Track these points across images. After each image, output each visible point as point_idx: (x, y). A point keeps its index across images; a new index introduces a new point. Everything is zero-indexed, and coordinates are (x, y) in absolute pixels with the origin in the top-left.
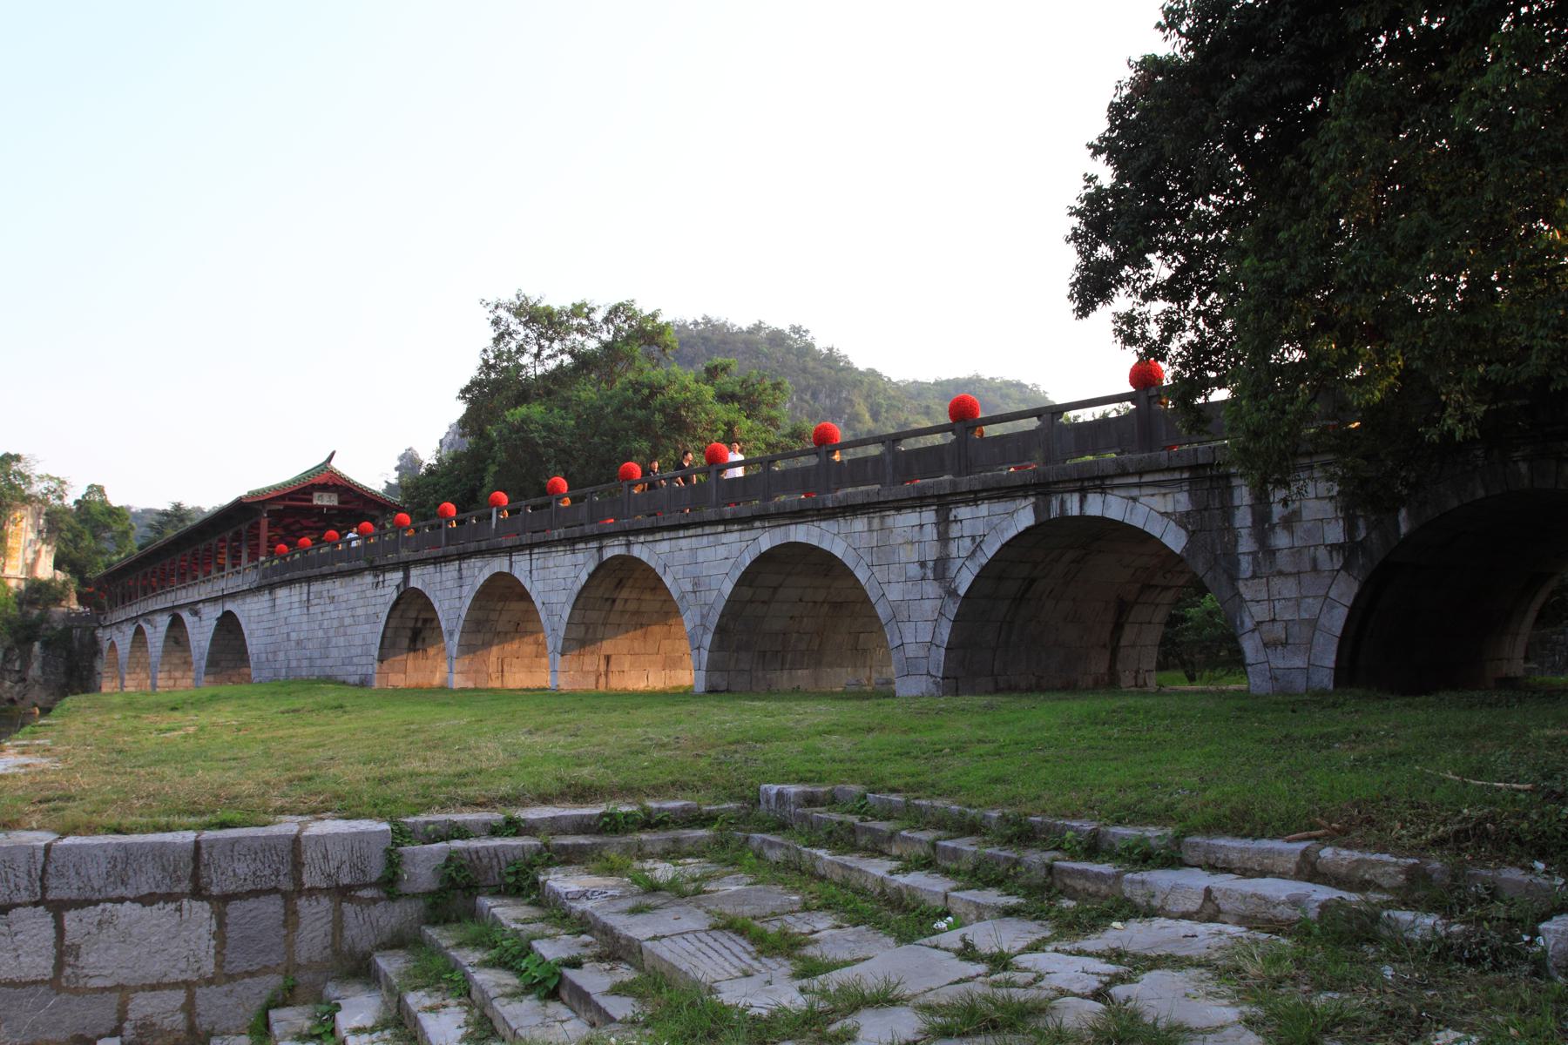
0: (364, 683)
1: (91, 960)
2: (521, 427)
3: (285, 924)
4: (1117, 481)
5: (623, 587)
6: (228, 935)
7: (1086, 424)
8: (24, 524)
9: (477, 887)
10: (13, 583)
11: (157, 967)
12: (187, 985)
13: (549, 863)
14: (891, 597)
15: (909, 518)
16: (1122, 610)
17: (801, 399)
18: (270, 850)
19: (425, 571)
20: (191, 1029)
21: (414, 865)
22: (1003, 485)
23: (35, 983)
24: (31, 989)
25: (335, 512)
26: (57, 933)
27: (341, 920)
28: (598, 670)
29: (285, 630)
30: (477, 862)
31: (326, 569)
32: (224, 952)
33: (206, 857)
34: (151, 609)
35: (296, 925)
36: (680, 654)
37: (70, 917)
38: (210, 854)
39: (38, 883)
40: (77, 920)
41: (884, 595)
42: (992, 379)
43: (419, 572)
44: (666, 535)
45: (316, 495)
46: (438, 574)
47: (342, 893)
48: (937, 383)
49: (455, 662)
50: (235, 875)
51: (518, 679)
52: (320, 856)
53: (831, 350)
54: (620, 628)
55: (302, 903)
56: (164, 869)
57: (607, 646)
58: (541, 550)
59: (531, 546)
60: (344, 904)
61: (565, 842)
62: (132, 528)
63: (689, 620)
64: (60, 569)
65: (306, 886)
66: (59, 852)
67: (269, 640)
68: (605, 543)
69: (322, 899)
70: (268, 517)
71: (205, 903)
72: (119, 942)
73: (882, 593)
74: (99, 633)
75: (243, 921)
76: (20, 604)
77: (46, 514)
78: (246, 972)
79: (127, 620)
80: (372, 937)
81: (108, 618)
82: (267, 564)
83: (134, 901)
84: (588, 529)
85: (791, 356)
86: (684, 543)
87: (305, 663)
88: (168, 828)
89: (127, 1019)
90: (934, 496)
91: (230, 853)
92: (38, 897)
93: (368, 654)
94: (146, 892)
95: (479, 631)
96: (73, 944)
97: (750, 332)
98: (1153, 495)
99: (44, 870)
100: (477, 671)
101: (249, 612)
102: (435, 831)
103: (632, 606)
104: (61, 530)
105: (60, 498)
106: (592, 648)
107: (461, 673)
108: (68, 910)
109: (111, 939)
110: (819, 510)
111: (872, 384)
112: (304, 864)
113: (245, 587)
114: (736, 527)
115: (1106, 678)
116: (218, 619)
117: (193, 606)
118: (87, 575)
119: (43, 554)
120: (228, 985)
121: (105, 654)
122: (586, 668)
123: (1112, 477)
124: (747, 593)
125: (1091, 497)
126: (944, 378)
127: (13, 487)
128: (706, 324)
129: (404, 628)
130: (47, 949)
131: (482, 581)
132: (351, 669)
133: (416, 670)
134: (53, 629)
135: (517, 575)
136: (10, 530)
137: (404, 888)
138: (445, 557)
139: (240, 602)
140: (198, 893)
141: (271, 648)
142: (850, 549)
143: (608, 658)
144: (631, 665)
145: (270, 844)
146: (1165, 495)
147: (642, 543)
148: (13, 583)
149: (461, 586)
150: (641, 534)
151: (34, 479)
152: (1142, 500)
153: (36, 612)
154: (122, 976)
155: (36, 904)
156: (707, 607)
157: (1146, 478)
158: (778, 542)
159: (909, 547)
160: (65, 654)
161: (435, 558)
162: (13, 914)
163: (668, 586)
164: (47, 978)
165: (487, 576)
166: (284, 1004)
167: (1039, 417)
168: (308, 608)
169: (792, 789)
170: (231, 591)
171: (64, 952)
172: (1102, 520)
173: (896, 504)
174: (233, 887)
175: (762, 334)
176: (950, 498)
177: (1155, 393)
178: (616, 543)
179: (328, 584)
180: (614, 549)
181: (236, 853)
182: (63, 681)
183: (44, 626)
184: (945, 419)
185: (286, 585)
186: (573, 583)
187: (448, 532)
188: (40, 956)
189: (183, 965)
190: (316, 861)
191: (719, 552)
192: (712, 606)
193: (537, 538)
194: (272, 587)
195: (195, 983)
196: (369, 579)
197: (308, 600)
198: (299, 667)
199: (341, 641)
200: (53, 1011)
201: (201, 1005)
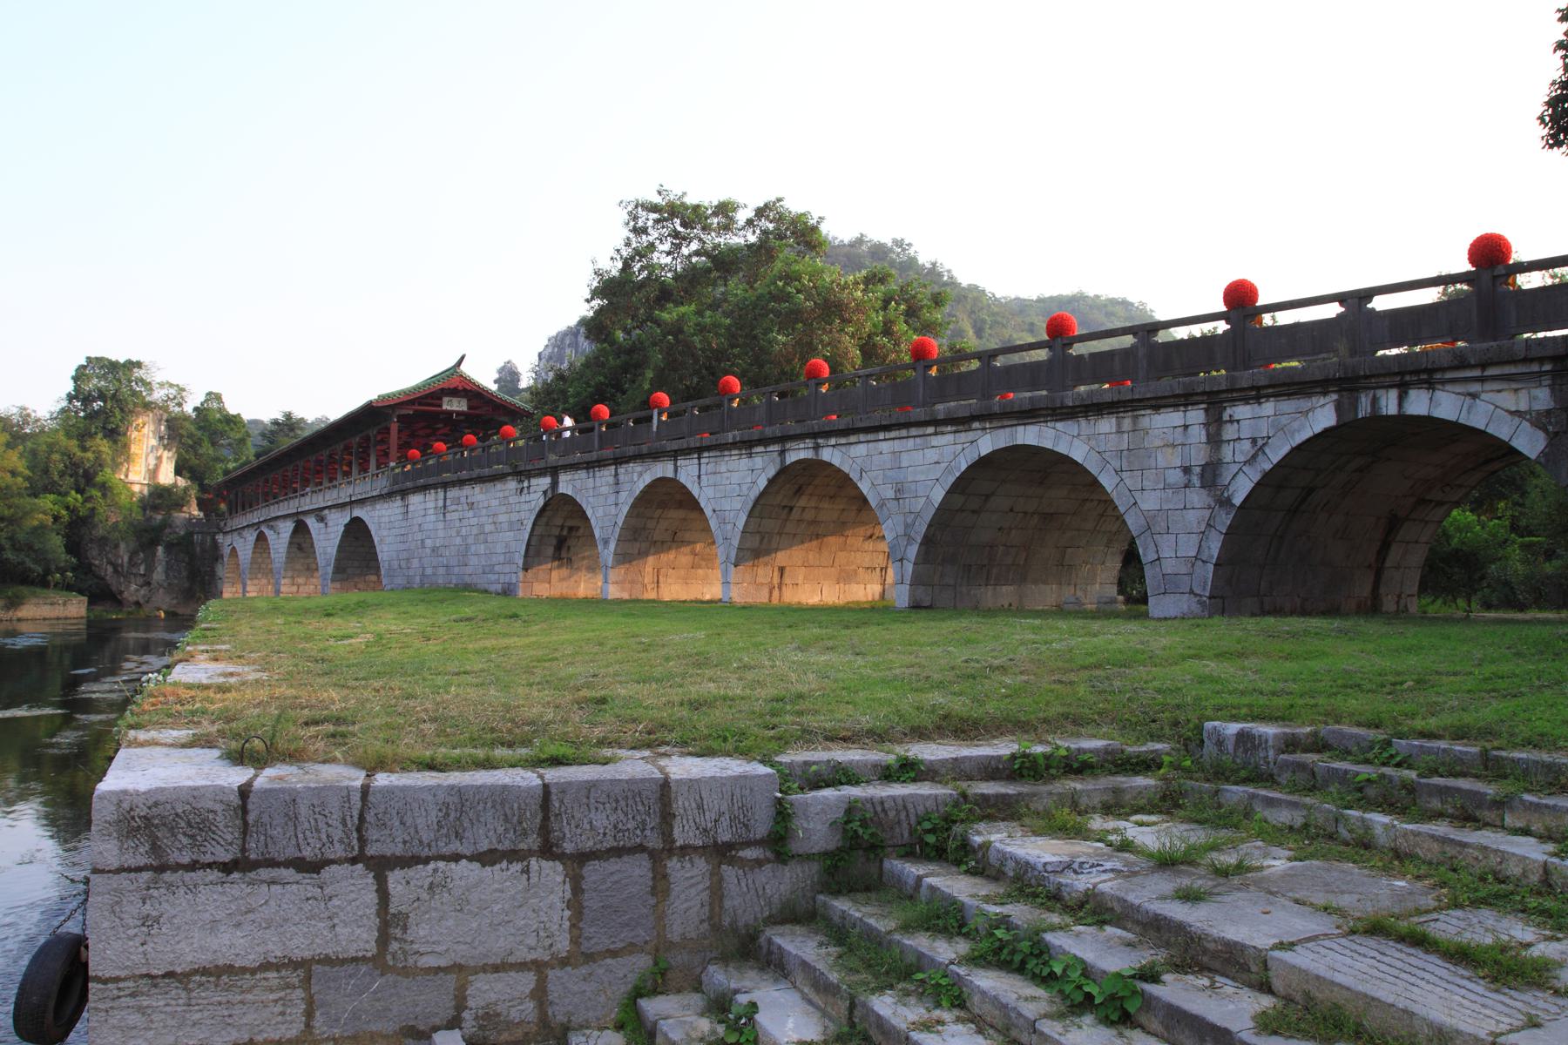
0: (507, 592)
1: (422, 933)
2: (677, 329)
3: (654, 891)
4: (1449, 375)
6: (585, 904)
7: (1182, 341)
8: (145, 430)
9: (882, 847)
11: (501, 943)
12: (538, 966)
13: (972, 818)
14: (1145, 507)
15: (1171, 418)
16: (1393, 524)
18: (633, 798)
19: (576, 477)
20: (544, 1021)
21: (807, 819)
22: (1297, 379)
23: (355, 960)
24: (351, 968)
25: (462, 418)
26: (380, 898)
27: (721, 888)
28: (771, 582)
29: (419, 536)
30: (882, 815)
31: (464, 474)
32: (581, 925)
33: (557, 805)
35: (666, 892)
36: (854, 567)
37: (395, 878)
38: (562, 802)
39: (355, 835)
40: (404, 882)
41: (1135, 503)
42: (1097, 297)
43: (569, 477)
44: (862, 437)
45: (446, 399)
46: (591, 480)
47: (721, 852)
48: (1040, 300)
49: (610, 571)
50: (592, 828)
51: (673, 590)
52: (694, 805)
53: (934, 264)
54: (796, 539)
55: (673, 864)
56: (506, 820)
57: (781, 558)
59: (700, 450)
60: (724, 867)
61: (985, 791)
62: (249, 436)
63: (890, 529)
65: (678, 844)
66: (379, 796)
67: (402, 547)
68: (788, 446)
69: (696, 860)
71: (557, 863)
72: (455, 910)
73: (1133, 501)
74: (220, 538)
75: (604, 887)
76: (144, 509)
77: (167, 421)
78: (608, 951)
80: (757, 909)
82: (397, 471)
83: (471, 859)
84: (769, 432)
86: (884, 446)
87: (441, 571)
88: (488, 764)
89: (466, 1008)
90: (1204, 393)
91: (585, 800)
92: (356, 853)
93: (510, 562)
94: (485, 848)
95: (635, 540)
96: (400, 913)
97: (852, 245)
98: (1499, 391)
99: (362, 818)
100: (632, 582)
101: (383, 520)
102: (817, 773)
103: (809, 515)
104: (182, 436)
105: (180, 405)
106: (766, 559)
108: (392, 870)
109: (445, 907)
110: (1054, 409)
111: (976, 299)
112: (674, 816)
113: (374, 494)
114: (949, 428)
115: (1369, 603)
117: (319, 513)
120: (586, 966)
122: (760, 580)
123: (1443, 370)
125: (1413, 393)
126: (1047, 295)
127: (134, 394)
130: (369, 918)
132: (493, 577)
135: (683, 480)
137: (795, 847)
138: (598, 461)
139: (369, 508)
140: (548, 850)
141: (405, 555)
142: (1093, 453)
143: (782, 570)
144: (805, 578)
145: (631, 792)
146: (1516, 390)
148: (136, 488)
151: (155, 386)
152: (1483, 396)
154: (462, 954)
155: (353, 861)
157: (1490, 372)
159: (1170, 450)
160: (187, 559)
161: (588, 463)
162: (327, 873)
163: (865, 492)
164: (369, 955)
166: (655, 992)
167: (1135, 334)
169: (1269, 730)
171: (389, 922)
172: (1428, 421)
173: (1153, 403)
174: (591, 843)
175: (864, 248)
176: (1224, 395)
177: (1503, 272)
179: (467, 490)
180: (799, 453)
181: (593, 801)
182: (187, 585)
184: (1221, 307)
187: (601, 435)
188: (359, 927)
189: (532, 941)
190: (689, 813)
192: (918, 515)
193: (707, 439)
194: (404, 493)
195: (546, 964)
196: (512, 484)
197: (445, 506)
199: (482, 548)
200: (379, 995)
201: (554, 990)
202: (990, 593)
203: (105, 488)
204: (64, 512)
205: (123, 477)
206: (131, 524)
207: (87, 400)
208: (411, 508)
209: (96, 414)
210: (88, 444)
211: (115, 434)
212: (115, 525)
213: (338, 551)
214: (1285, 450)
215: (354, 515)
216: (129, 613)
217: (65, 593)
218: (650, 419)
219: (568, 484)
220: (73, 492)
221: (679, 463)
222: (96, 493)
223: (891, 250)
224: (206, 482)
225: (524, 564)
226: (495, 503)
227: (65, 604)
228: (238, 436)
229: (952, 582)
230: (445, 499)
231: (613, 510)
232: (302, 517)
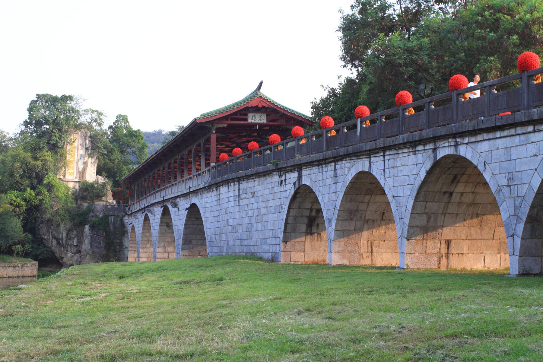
0: (273, 259)
5: (458, 182)
8: (76, 144)
10: (71, 185)
19: (312, 172)
28: (439, 253)
34: (152, 202)
43: (308, 172)
44: (486, 136)
45: (250, 115)
49: (332, 242)
54: (457, 218)
57: (447, 233)
58: (392, 152)
59: (384, 149)
64: (100, 175)
67: (217, 225)
68: (438, 145)
70: (216, 132)
74: (126, 219)
77: (90, 137)
81: (131, 209)
86: (500, 143)
87: (238, 243)
93: (276, 237)
95: (351, 219)
100: (351, 252)
103: (468, 199)
104: (100, 148)
105: (100, 125)
106: (434, 233)
113: (202, 186)
117: (174, 201)
119: (89, 164)
121: (129, 234)
122: (429, 251)
129: (302, 216)
132: (266, 248)
133: (313, 249)
134: (97, 216)
135: (374, 173)
136: (68, 148)
139: (200, 197)
141: (218, 231)
143: (448, 243)
144: (469, 249)
147: (467, 144)
148: (71, 185)
149: (336, 183)
150: (465, 136)
151: (81, 113)
153: (86, 205)
156: (520, 200)
161: (318, 161)
168: (239, 200)
170: (194, 189)
178: (447, 144)
183: (91, 214)
187: (328, 140)
191: (529, 150)
192: (523, 199)
193: (388, 142)
196: (276, 178)
197: (239, 195)
199: (259, 226)
203: (50, 187)
204: (23, 203)
205: (62, 177)
206: (68, 211)
207: (38, 124)
208: (221, 197)
210: (38, 155)
211: (54, 148)
212: (57, 212)
213: (185, 228)
215: (192, 202)
217: (23, 259)
218: (355, 126)
220: (28, 189)
221: (372, 159)
224: (117, 179)
225: (284, 238)
226: (266, 192)
228: (140, 146)
230: (239, 190)
231: (334, 197)
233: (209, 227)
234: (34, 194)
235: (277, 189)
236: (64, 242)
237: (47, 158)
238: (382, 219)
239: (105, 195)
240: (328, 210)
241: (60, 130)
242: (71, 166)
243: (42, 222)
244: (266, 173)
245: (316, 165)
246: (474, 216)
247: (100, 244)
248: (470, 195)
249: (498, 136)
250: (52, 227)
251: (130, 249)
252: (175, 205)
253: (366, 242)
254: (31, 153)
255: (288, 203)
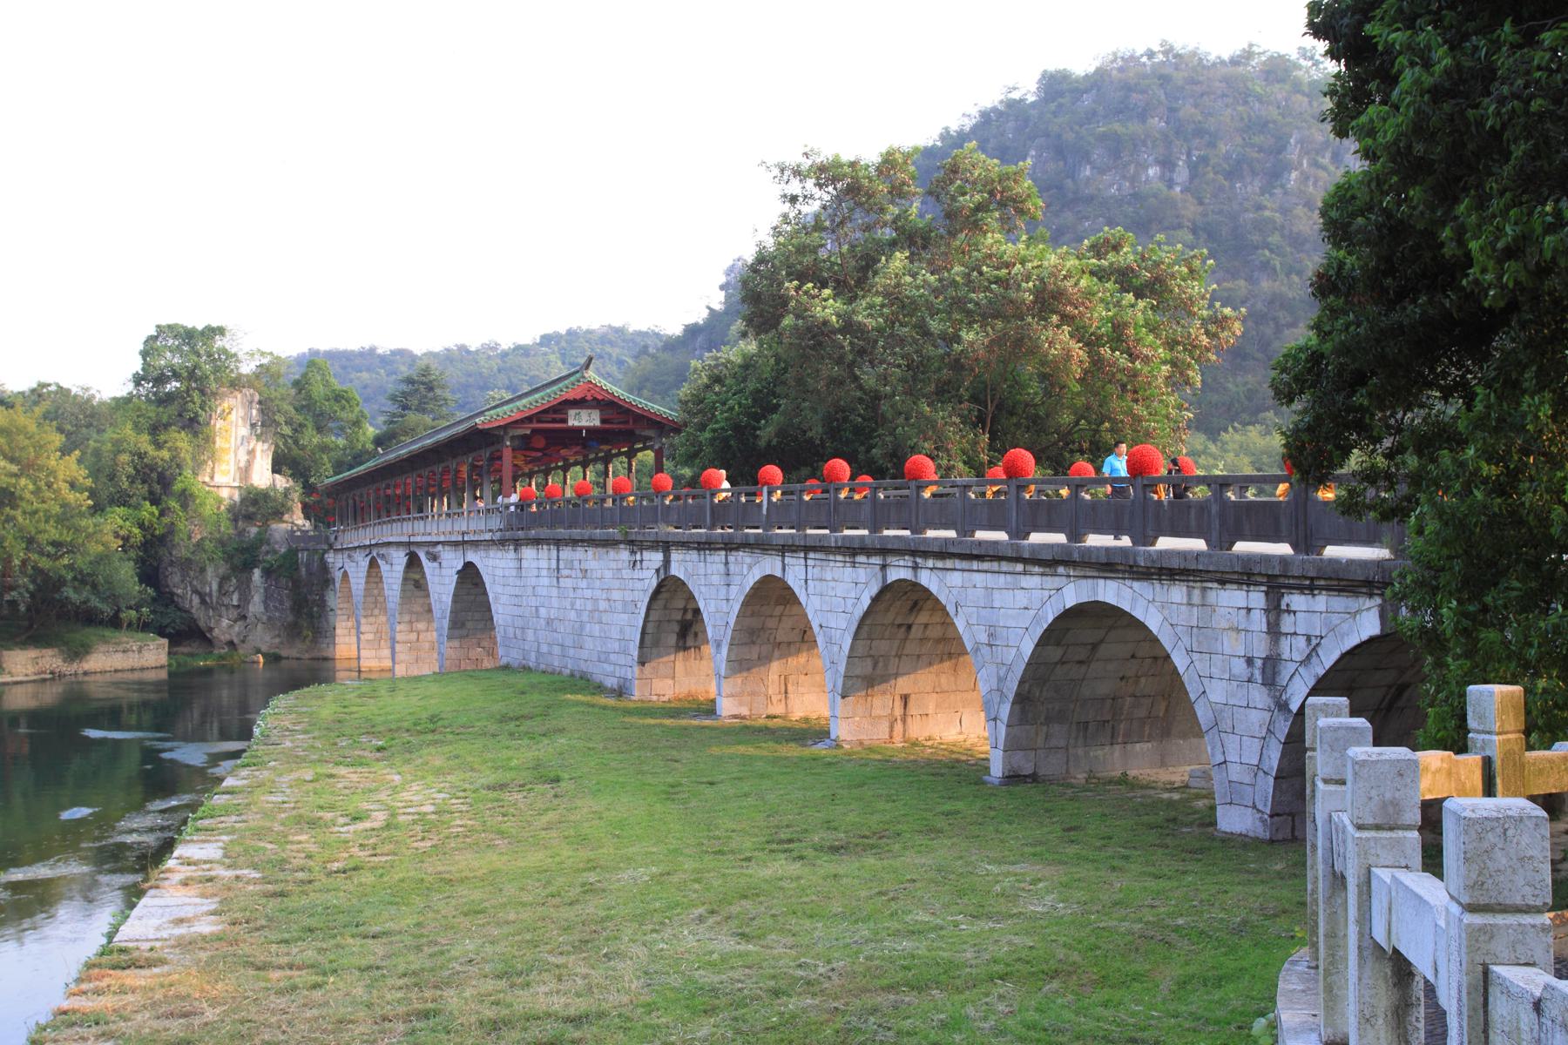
0: (620, 692)
5: (920, 610)
8: (233, 417)
17: (1315, 164)
19: (688, 558)
28: (892, 714)
29: (533, 602)
43: (681, 557)
44: (958, 564)
54: (921, 661)
57: (903, 684)
74: (330, 557)
76: (235, 520)
77: (260, 402)
79: (359, 547)
85: (1299, 97)
86: (978, 577)
93: (625, 652)
95: (753, 643)
97: (1235, 62)
100: (753, 694)
101: (495, 566)
104: (278, 424)
107: (732, 696)
116: (458, 572)
118: (312, 480)
119: (258, 453)
121: (337, 585)
124: (1054, 653)
128: (1166, 53)
131: (751, 584)
132: (609, 668)
133: (687, 673)
134: (275, 552)
135: (790, 583)
136: (218, 426)
139: (482, 553)
141: (519, 622)
142: (1166, 623)
143: (905, 699)
148: (225, 493)
151: (241, 355)
158: (1085, 598)
159: (1234, 634)
165: (757, 578)
178: (902, 563)
180: (899, 571)
182: (290, 618)
183: (264, 548)
185: (532, 544)
186: (855, 605)
194: (517, 544)
196: (624, 555)
197: (558, 569)
198: (550, 653)
202: (1117, 754)
203: (186, 498)
204: (136, 531)
205: (207, 479)
206: (221, 543)
207: (160, 380)
208: (525, 564)
209: (169, 398)
211: (194, 425)
212: (199, 545)
214: (1335, 656)
215: (468, 559)
216: (222, 657)
217: (141, 635)
219: (683, 565)
221: (787, 560)
222: (173, 504)
223: (1297, 67)
225: (640, 656)
226: (608, 574)
227: (140, 651)
228: (352, 416)
229: (1062, 743)
231: (724, 606)
232: (413, 548)
233: (502, 611)
234: (157, 513)
235: (627, 573)
236: (214, 599)
237: (179, 444)
238: (803, 640)
239: (289, 510)
240: (714, 626)
241: (203, 392)
242: (226, 458)
243: (172, 563)
244: (608, 543)
245: (694, 549)
246: (945, 657)
247: (281, 602)
248: (939, 627)
249: (975, 568)
250: (192, 573)
251: (339, 612)
252: (434, 558)
253: (776, 677)
254: (149, 434)
255: (647, 600)
